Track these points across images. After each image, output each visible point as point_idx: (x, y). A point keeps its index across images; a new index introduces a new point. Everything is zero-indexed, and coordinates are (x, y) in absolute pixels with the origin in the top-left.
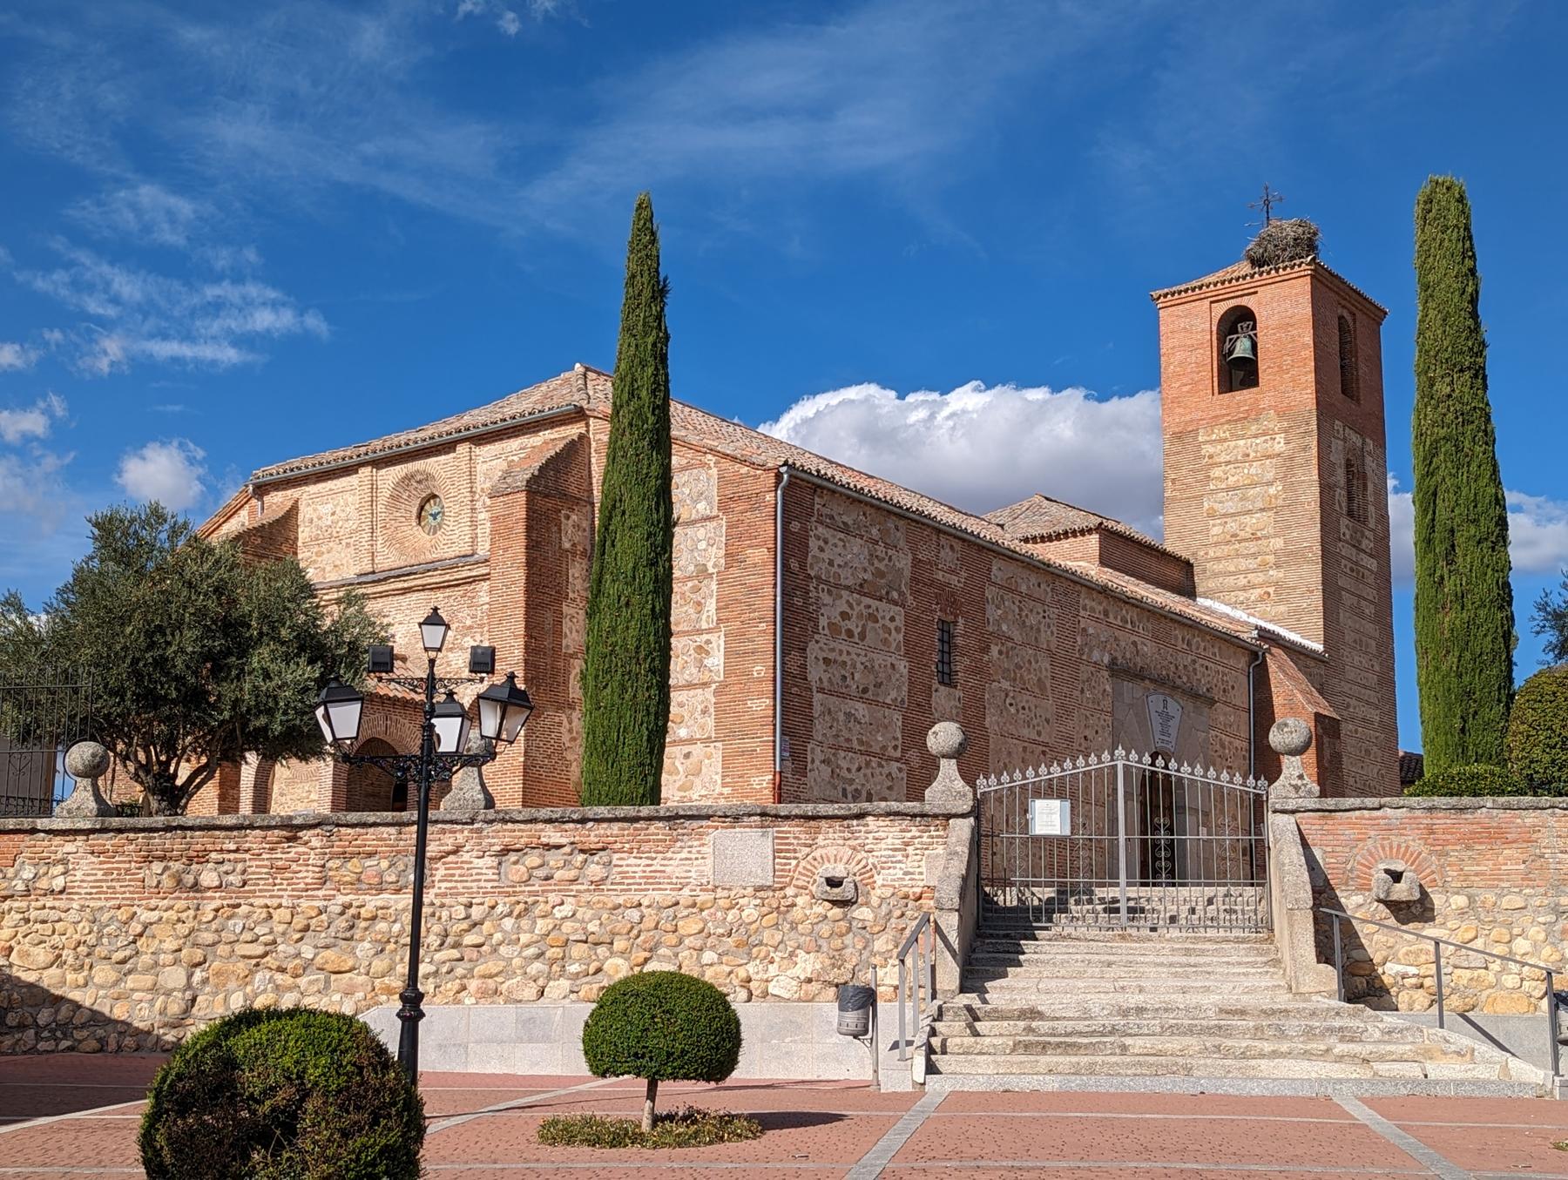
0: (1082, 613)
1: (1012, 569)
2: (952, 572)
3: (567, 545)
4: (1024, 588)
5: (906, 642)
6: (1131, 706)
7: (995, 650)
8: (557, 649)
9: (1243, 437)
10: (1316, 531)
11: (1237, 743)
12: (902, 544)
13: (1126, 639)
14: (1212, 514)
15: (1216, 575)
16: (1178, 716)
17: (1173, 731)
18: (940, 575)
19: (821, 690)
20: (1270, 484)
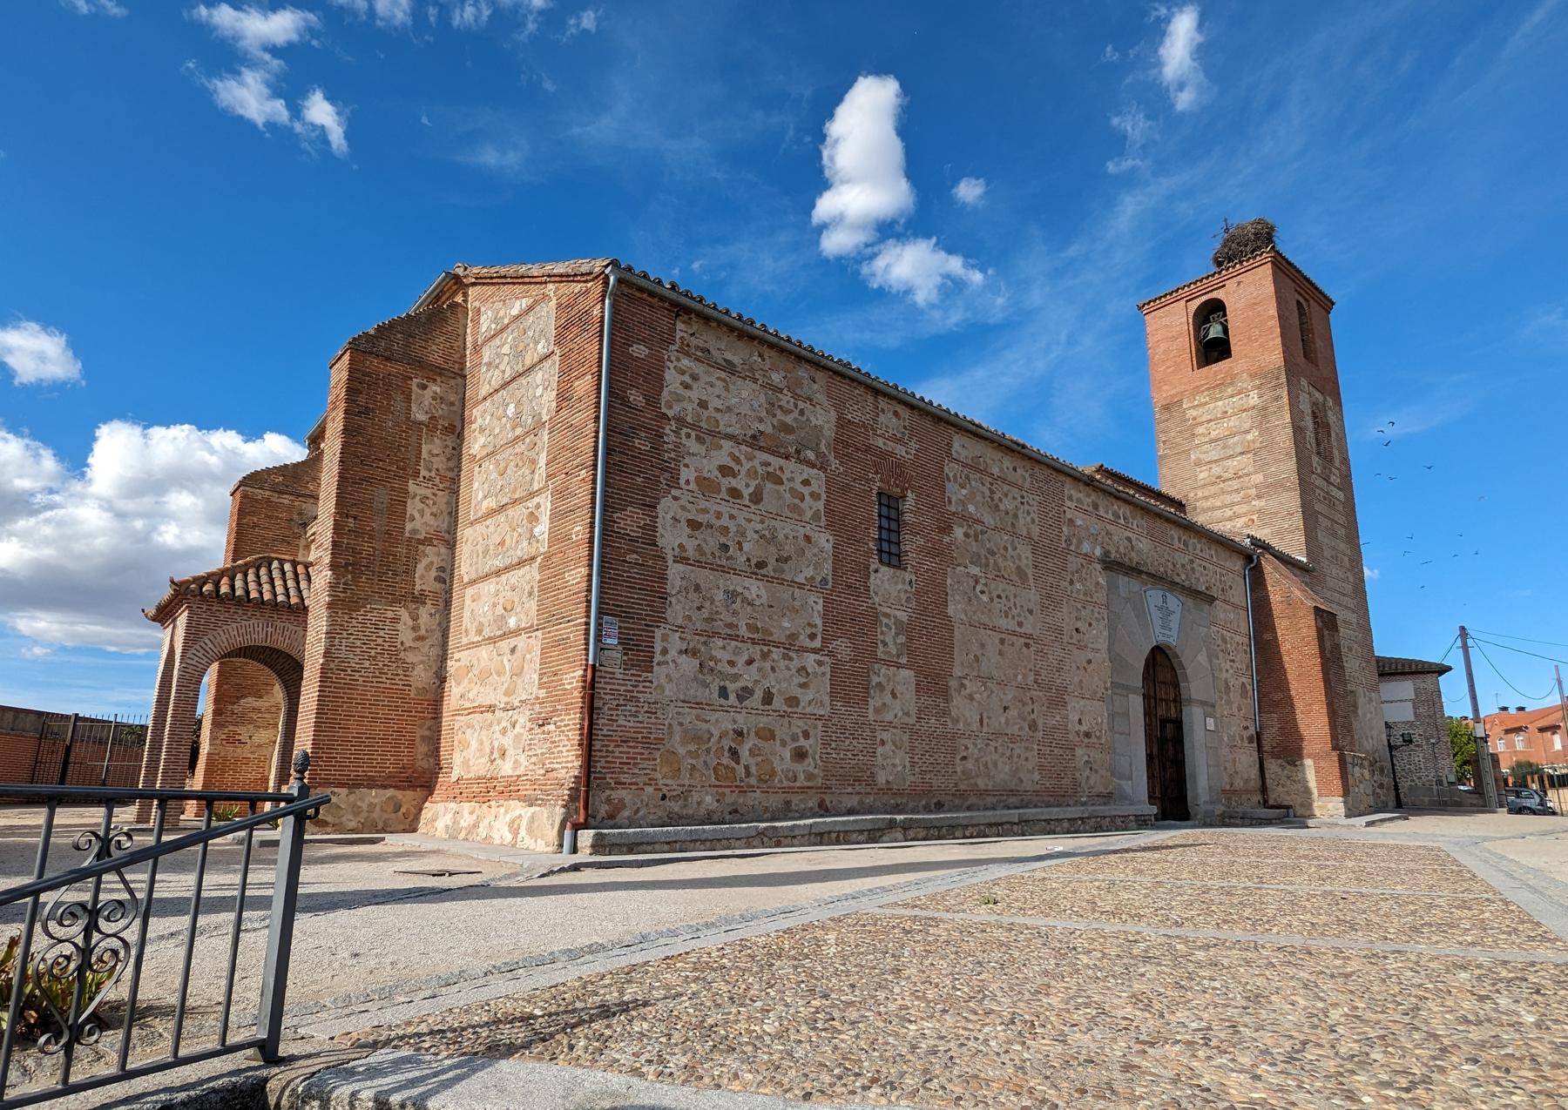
0: (1068, 503)
1: (977, 448)
2: (899, 441)
3: (421, 417)
4: (995, 471)
5: (829, 511)
6: (1127, 600)
7: (959, 532)
8: (393, 534)
9: (1220, 399)
10: (1292, 464)
11: (1238, 638)
12: (820, 397)
13: (1119, 534)
14: (1198, 463)
15: (1205, 511)
16: (1178, 610)
17: (1174, 625)
18: (880, 442)
19: (682, 559)
20: (1247, 432)
